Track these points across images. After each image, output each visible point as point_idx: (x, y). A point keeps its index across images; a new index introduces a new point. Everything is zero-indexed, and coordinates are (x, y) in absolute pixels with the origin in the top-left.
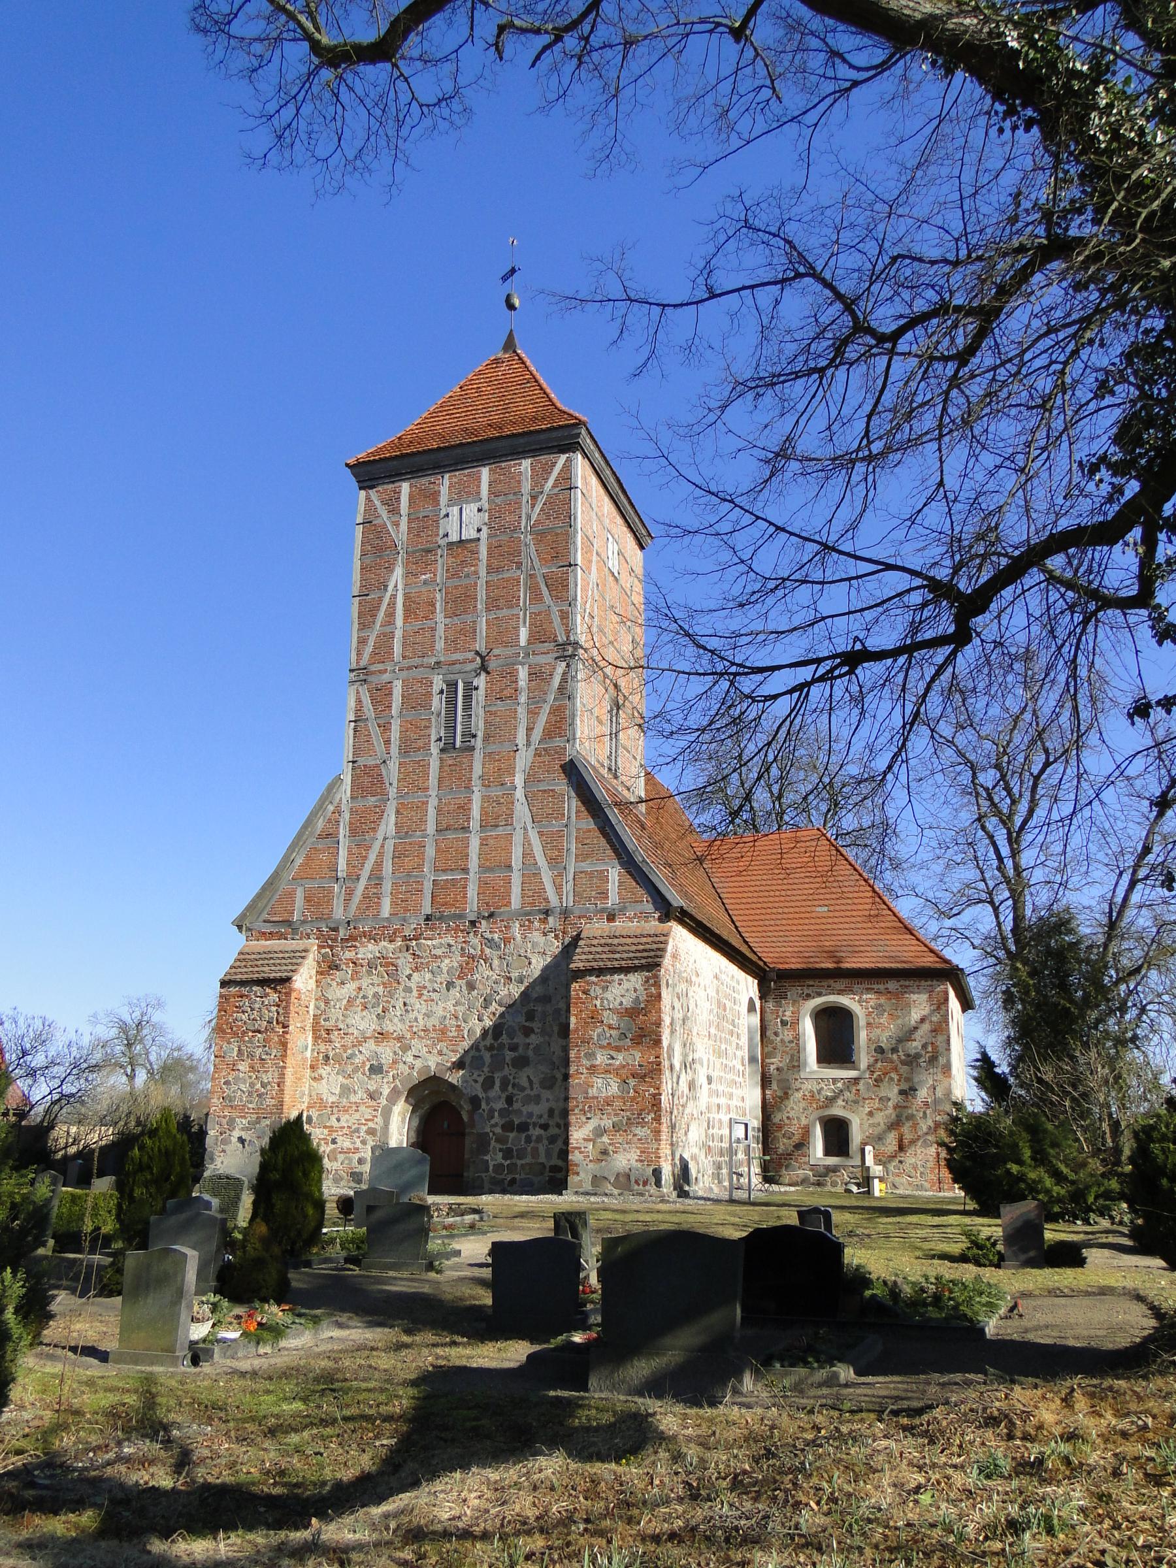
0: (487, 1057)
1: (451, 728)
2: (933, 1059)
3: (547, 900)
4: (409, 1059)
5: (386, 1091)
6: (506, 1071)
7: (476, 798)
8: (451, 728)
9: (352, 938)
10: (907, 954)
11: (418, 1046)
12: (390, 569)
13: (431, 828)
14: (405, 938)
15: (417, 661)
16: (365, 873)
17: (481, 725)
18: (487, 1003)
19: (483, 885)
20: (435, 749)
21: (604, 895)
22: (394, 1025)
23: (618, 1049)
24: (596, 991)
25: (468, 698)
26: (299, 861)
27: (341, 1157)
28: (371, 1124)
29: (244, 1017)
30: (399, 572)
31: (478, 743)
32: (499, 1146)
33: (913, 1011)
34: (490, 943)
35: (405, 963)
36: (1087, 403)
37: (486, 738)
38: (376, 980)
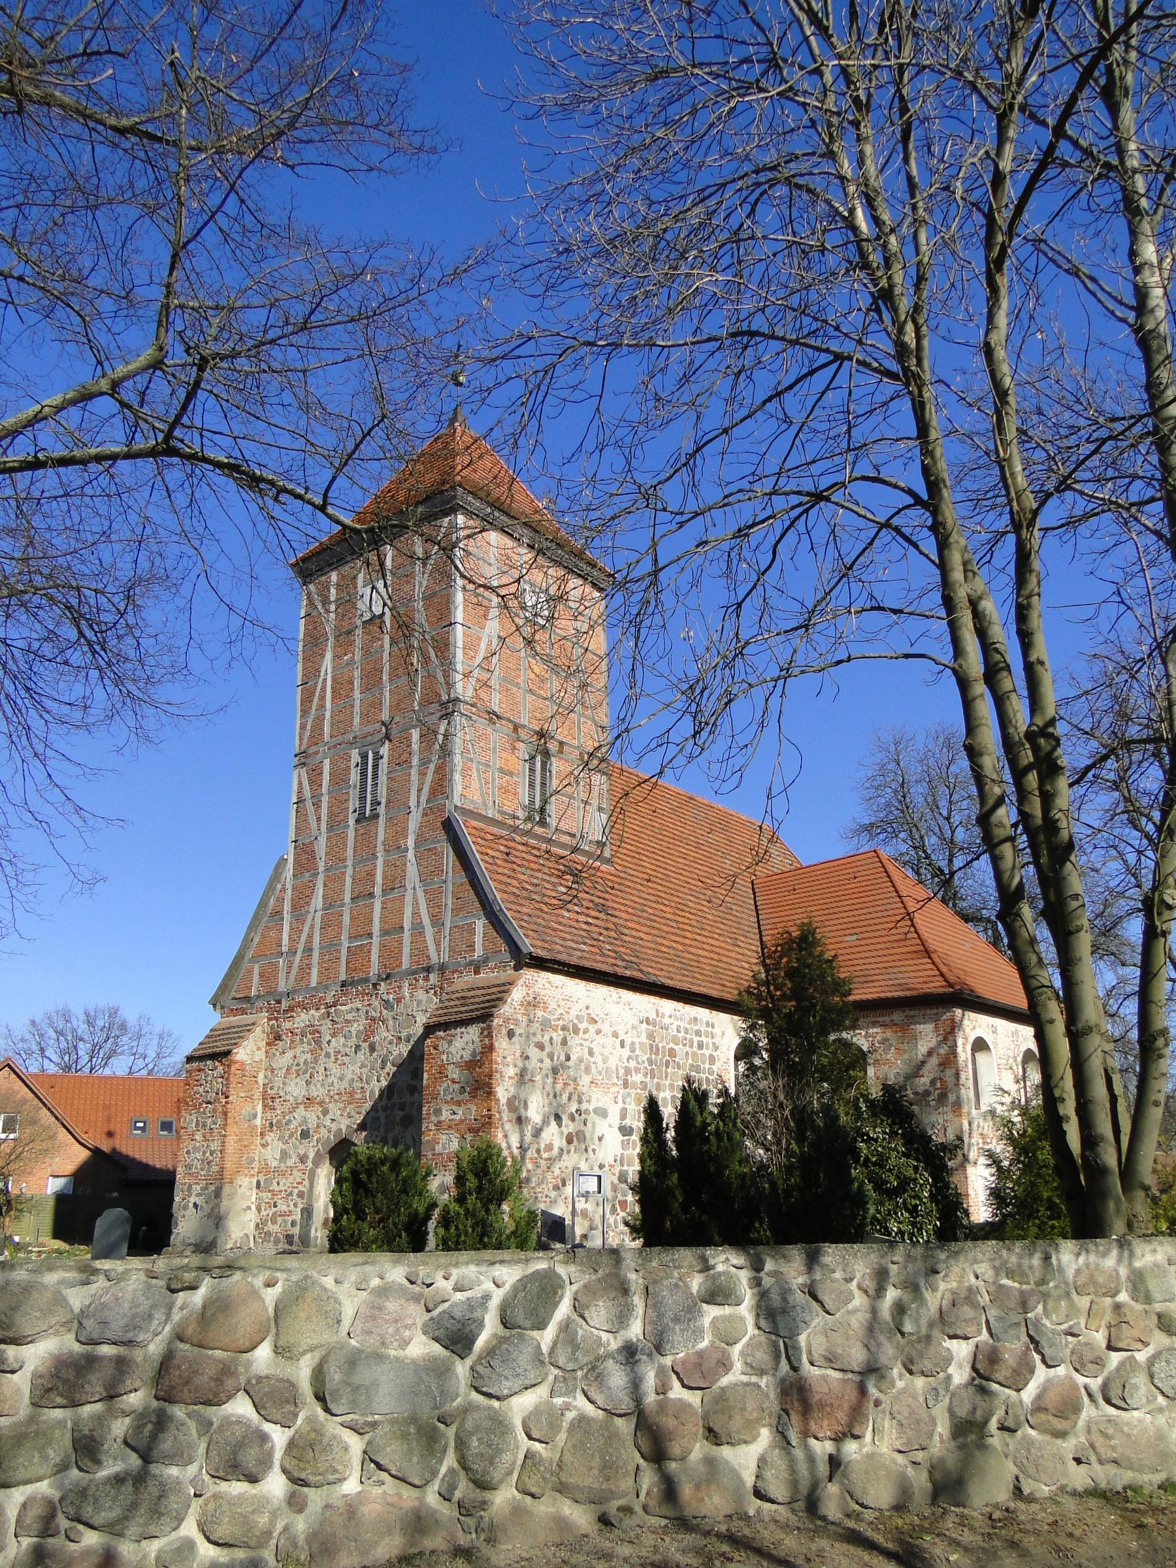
0: (382, 1116)
1: (363, 799)
2: (942, 1098)
3: (428, 957)
4: (328, 1123)
5: (311, 1155)
7: (380, 863)
8: (363, 799)
9: (291, 1009)
10: (920, 978)
11: (334, 1110)
12: (322, 656)
13: (347, 899)
14: (328, 1006)
16: (301, 947)
18: (384, 1063)
19: (383, 946)
20: (351, 822)
21: (471, 947)
22: (317, 1091)
23: (458, 1103)
24: (443, 1045)
25: (376, 766)
26: (256, 940)
27: (280, 1220)
28: (301, 1188)
29: (201, 1089)
30: (329, 656)
31: (381, 810)
33: (920, 1043)
34: (387, 1005)
35: (326, 1028)
37: (388, 802)
38: (306, 1047)
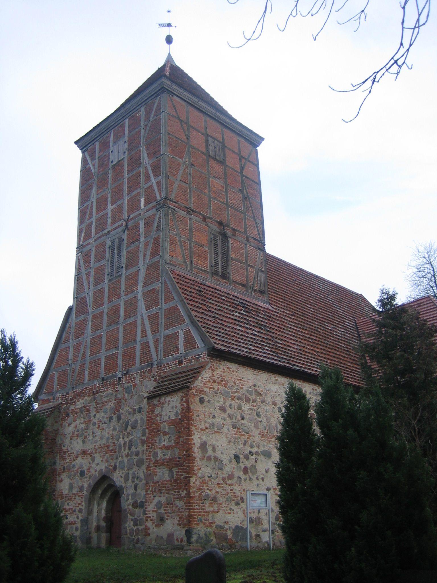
6: (134, 469)
11: (98, 458)
15: (101, 233)
17: (125, 261)
32: (131, 517)
36: (433, 290)
